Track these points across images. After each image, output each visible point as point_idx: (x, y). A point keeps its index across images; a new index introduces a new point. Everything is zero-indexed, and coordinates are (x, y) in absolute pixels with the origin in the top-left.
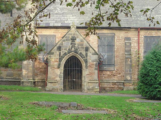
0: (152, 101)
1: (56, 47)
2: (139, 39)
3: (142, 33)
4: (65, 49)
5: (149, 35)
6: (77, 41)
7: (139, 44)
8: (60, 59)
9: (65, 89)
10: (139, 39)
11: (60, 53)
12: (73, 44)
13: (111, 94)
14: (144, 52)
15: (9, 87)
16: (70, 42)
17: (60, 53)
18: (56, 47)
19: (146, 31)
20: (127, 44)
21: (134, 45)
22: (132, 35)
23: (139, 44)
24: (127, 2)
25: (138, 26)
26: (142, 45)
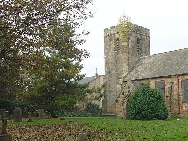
0: (143, 121)
1: (121, 94)
2: (178, 83)
3: (181, 78)
4: (125, 94)
5: (185, 79)
6: (131, 88)
7: (178, 86)
8: (123, 100)
9: (128, 118)
10: (178, 83)
11: (123, 96)
12: (129, 91)
13: (21, 112)
14: (182, 91)
15: (108, 118)
16: (128, 89)
17: (123, 96)
18: (121, 94)
19: (182, 76)
20: (169, 87)
21: (175, 87)
22: (174, 80)
23: (178, 86)
24: (89, 53)
25: (177, 74)
26: (180, 86)
